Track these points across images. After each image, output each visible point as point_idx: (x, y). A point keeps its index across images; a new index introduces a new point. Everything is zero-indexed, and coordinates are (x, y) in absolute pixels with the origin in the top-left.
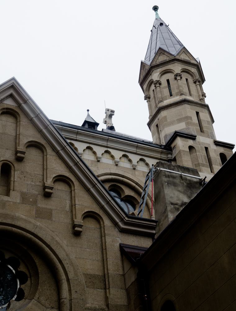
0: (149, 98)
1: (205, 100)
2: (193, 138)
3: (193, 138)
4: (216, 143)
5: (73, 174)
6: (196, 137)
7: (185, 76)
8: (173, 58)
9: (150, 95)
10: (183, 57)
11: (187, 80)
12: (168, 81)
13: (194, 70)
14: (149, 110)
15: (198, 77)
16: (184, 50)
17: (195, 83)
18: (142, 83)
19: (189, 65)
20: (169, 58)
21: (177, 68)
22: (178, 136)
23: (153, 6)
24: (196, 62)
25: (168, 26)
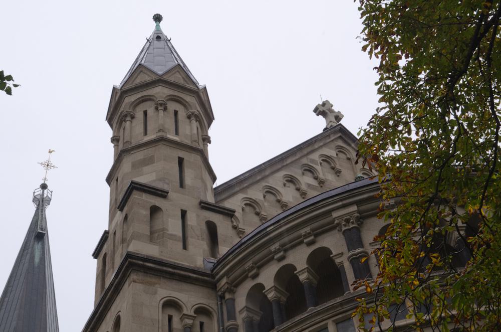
0: (118, 141)
1: (209, 148)
2: (163, 194)
3: (163, 194)
4: (202, 204)
5: (210, 211)
6: (168, 193)
7: (172, 106)
8: (154, 78)
9: (119, 137)
10: (177, 78)
11: (176, 113)
12: (145, 113)
13: (189, 98)
14: (214, 174)
15: (197, 109)
16: (181, 69)
17: (189, 117)
18: (110, 120)
19: (182, 91)
20: (150, 78)
21: (160, 92)
22: (136, 189)
23: (158, 13)
24: (196, 88)
25: (169, 41)
